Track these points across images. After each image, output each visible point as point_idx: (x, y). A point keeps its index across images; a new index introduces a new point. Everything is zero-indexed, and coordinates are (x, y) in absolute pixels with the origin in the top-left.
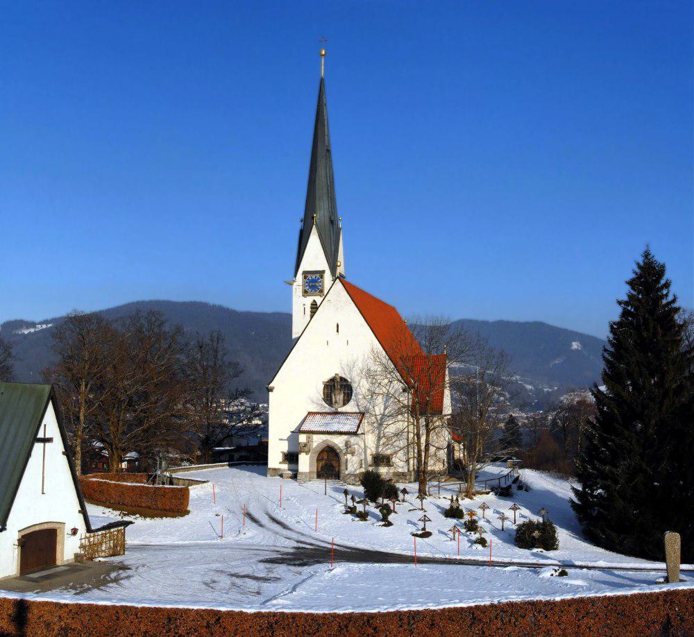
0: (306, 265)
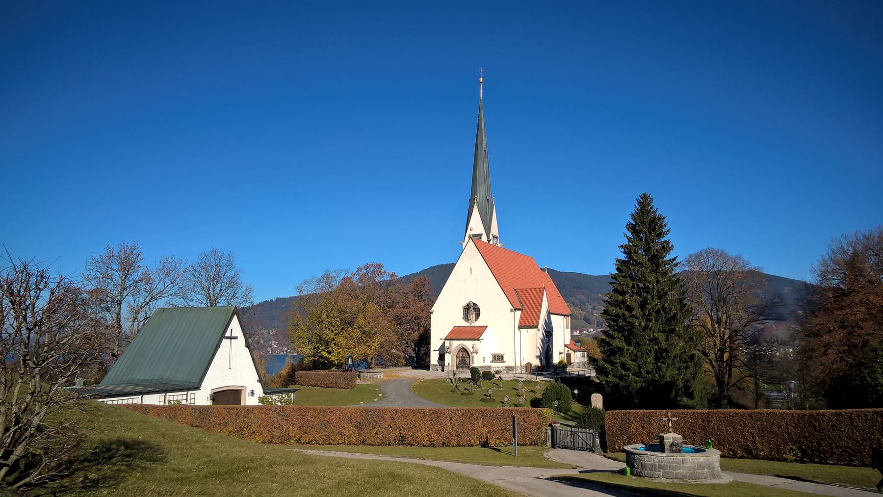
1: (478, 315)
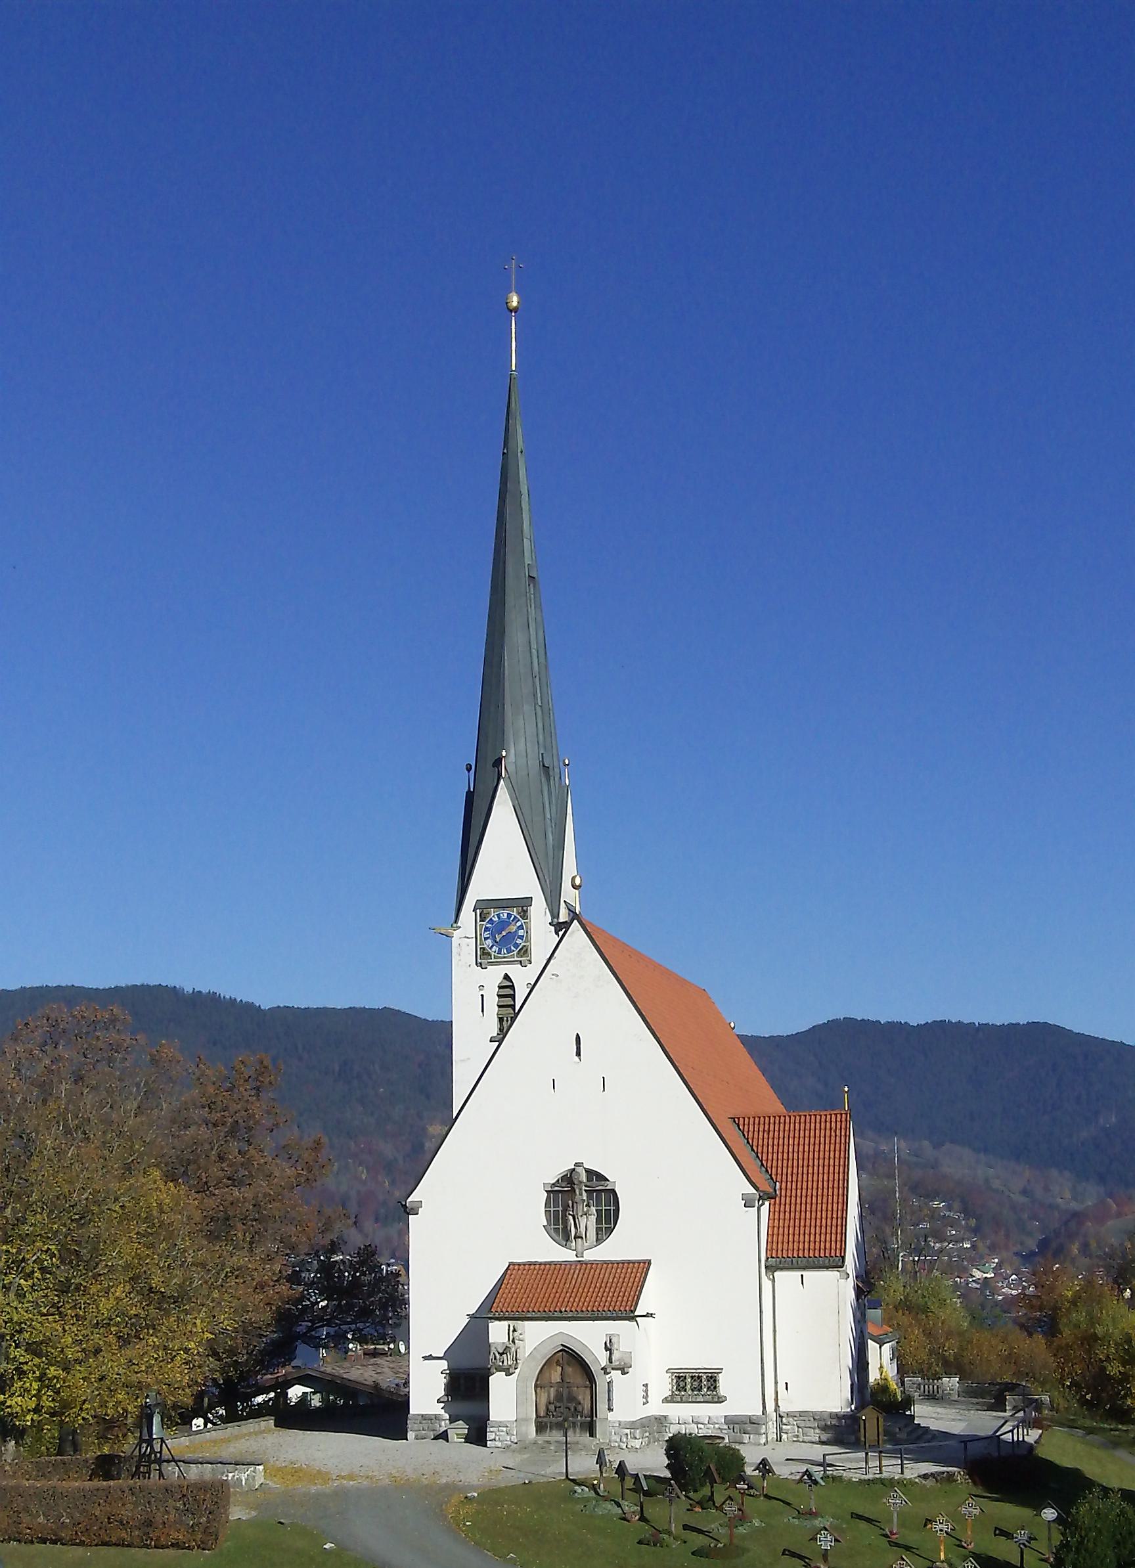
0: (482, 887)
1: (609, 1219)
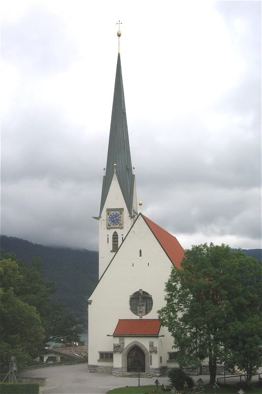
0: (109, 204)
